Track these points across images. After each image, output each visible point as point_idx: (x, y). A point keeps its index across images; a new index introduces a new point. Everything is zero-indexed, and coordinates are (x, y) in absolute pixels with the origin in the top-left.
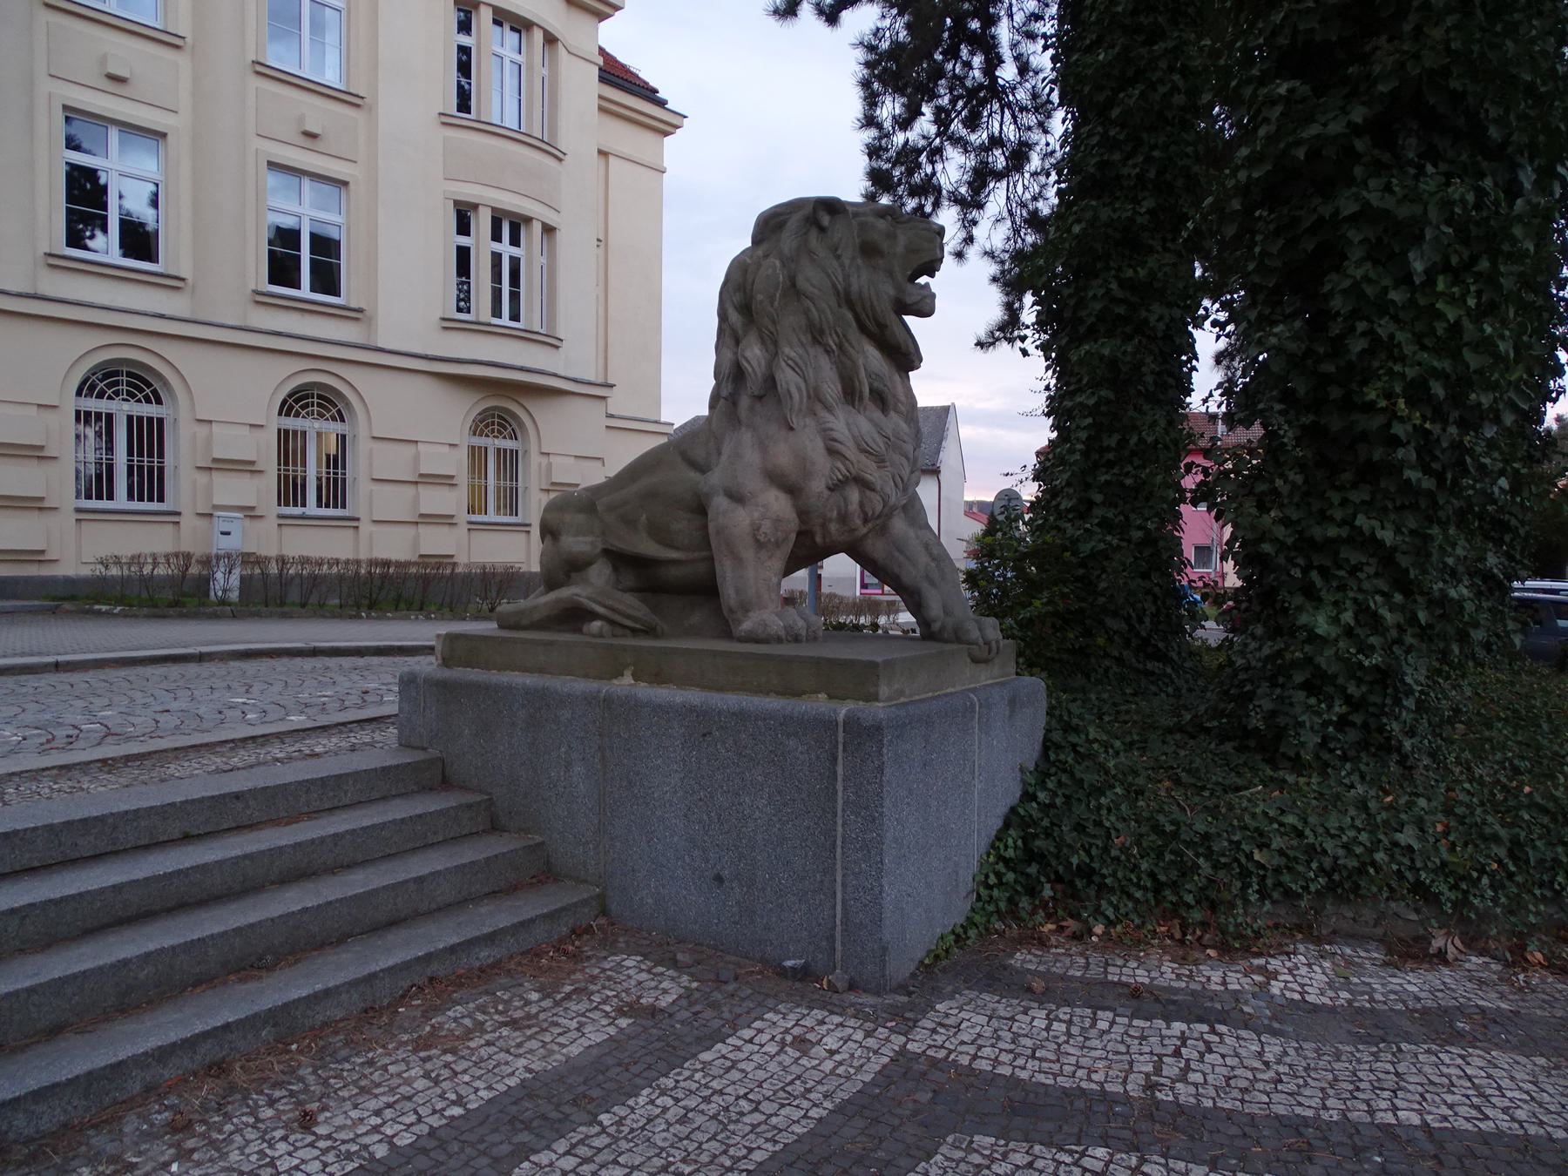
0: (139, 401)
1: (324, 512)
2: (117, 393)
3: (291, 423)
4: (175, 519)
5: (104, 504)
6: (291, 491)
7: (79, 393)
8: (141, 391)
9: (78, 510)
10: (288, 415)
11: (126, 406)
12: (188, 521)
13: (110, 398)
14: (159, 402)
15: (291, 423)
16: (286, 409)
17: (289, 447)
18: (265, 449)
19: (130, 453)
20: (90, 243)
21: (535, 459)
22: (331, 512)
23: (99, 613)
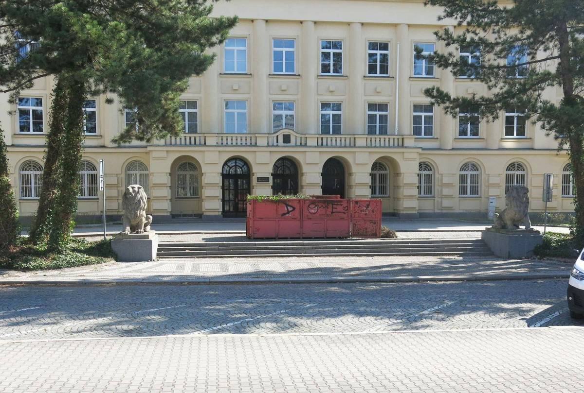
0: (35, 170)
1: (472, 196)
2: (30, 169)
3: (509, 172)
4: (480, 199)
5: (465, 196)
6: (463, 190)
7: (460, 170)
8: (427, 168)
9: (460, 197)
10: (565, 171)
11: (424, 172)
12: (483, 199)
13: (28, 170)
14: (478, 170)
15: (509, 172)
16: (508, 169)
17: (463, 179)
18: (456, 181)
19: (471, 183)
20: (540, 123)
21: (437, 176)
22: (91, 197)
23: (91, 227)
